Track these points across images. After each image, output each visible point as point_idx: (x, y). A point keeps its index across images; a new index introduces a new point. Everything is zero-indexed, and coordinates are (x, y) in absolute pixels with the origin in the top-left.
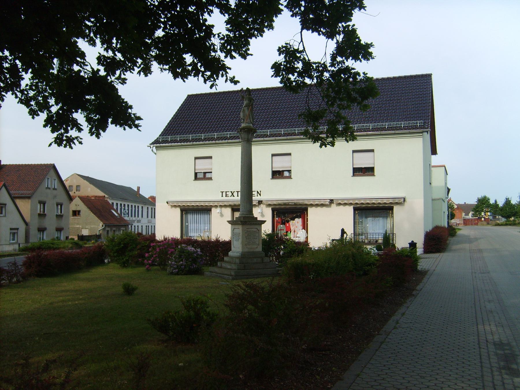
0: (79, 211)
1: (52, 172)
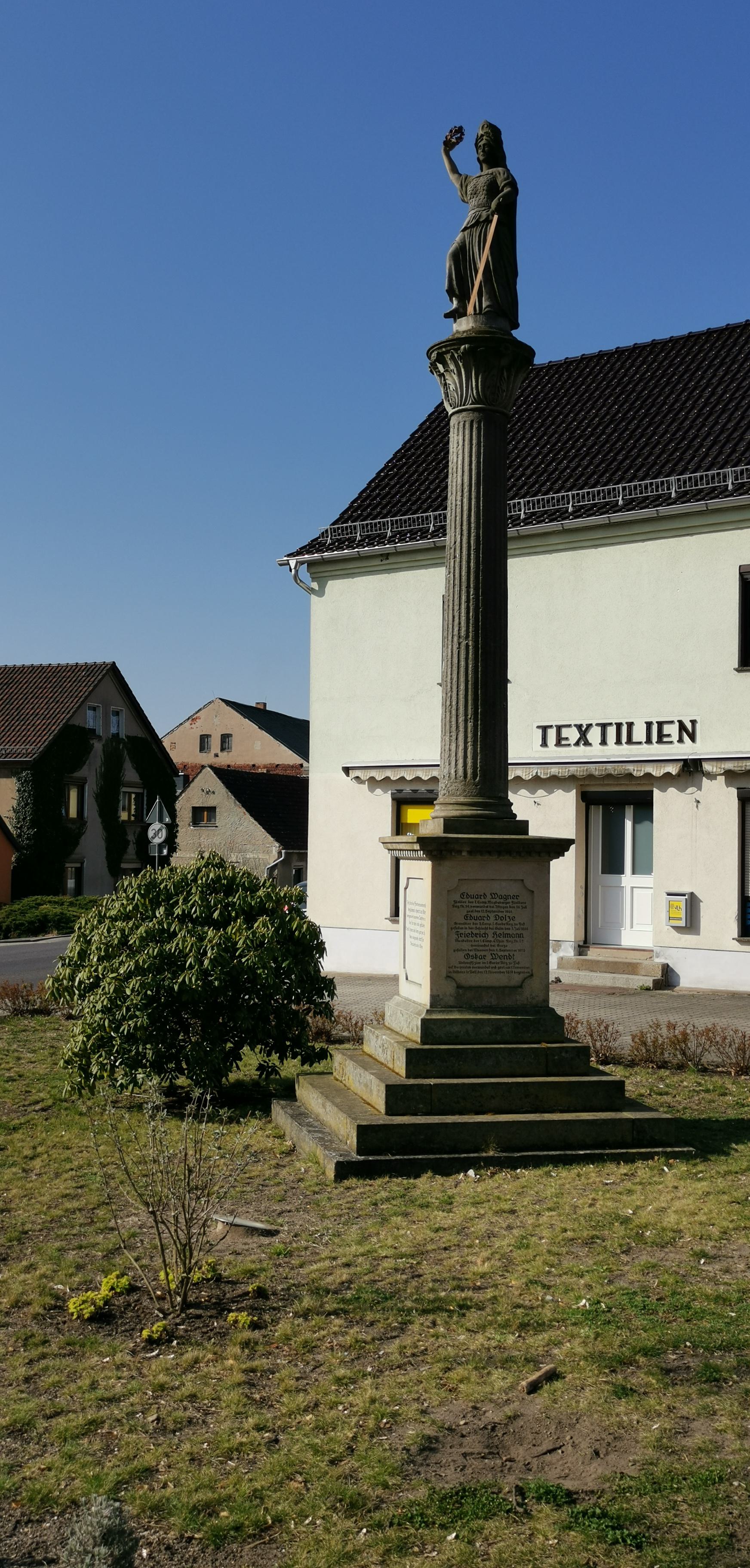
0: (212, 810)
1: (109, 687)
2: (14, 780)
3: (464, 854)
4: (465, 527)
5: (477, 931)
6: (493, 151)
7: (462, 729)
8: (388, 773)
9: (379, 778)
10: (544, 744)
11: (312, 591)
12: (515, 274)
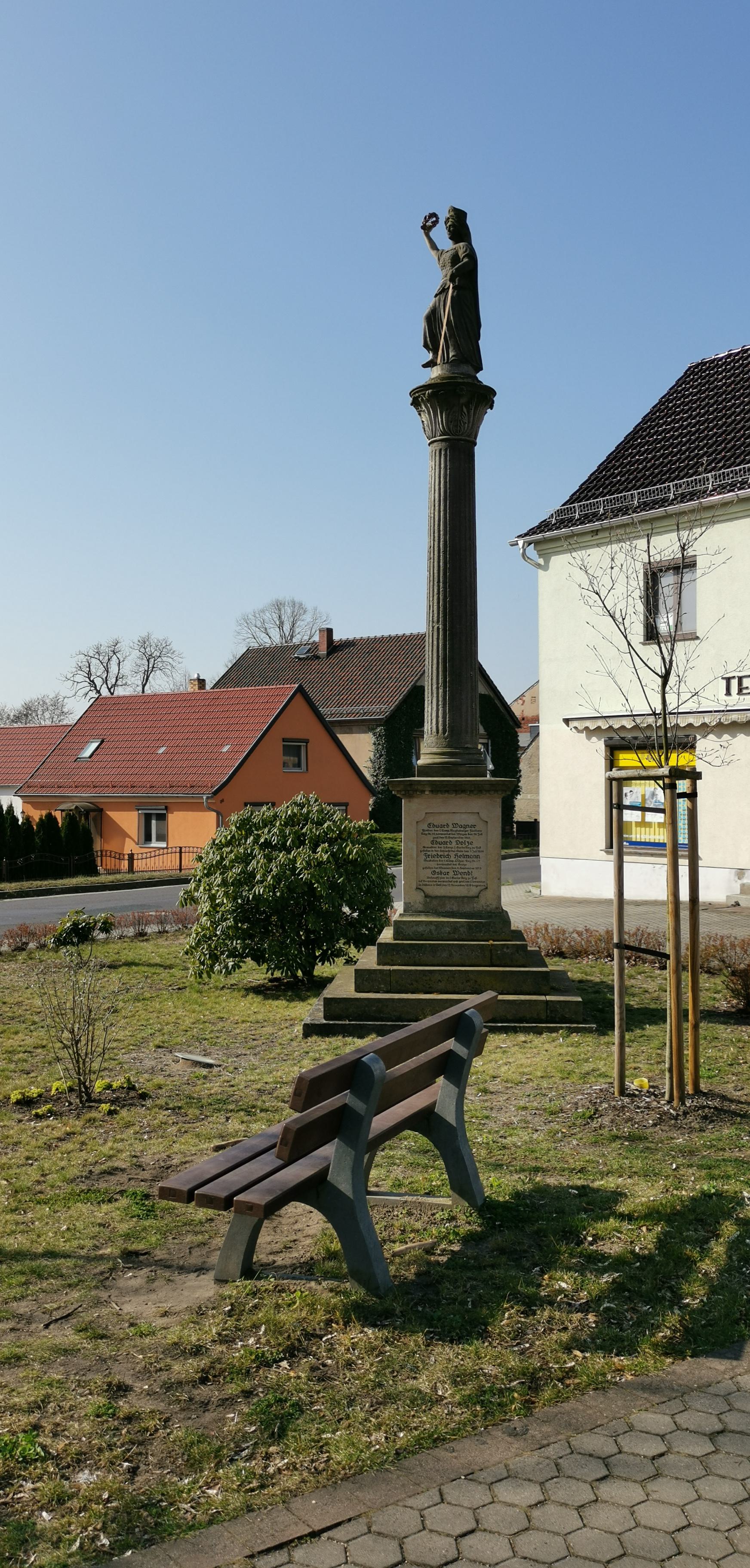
2: (370, 735)
3: (427, 793)
4: (436, 535)
5: (442, 853)
6: (459, 227)
7: (435, 695)
8: (588, 724)
9: (592, 728)
10: (728, 693)
11: (539, 566)
12: (479, 325)
